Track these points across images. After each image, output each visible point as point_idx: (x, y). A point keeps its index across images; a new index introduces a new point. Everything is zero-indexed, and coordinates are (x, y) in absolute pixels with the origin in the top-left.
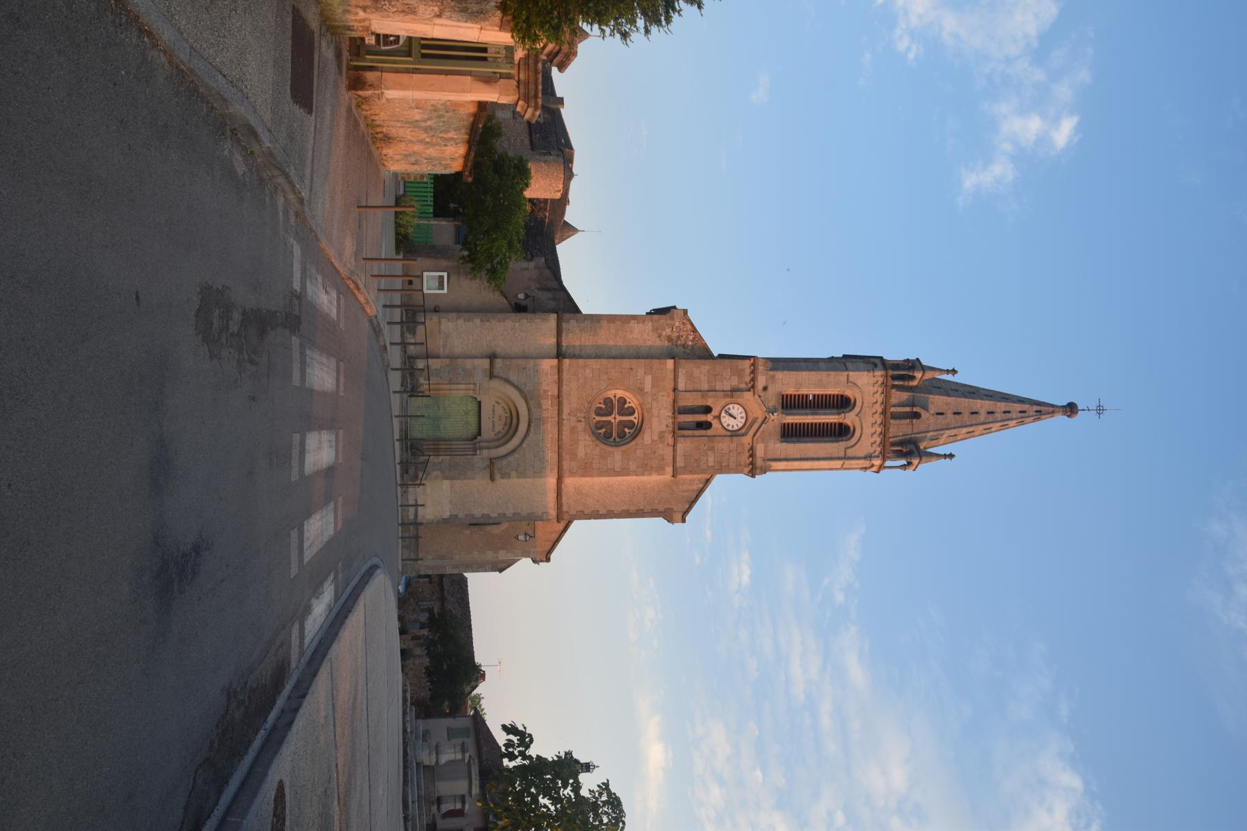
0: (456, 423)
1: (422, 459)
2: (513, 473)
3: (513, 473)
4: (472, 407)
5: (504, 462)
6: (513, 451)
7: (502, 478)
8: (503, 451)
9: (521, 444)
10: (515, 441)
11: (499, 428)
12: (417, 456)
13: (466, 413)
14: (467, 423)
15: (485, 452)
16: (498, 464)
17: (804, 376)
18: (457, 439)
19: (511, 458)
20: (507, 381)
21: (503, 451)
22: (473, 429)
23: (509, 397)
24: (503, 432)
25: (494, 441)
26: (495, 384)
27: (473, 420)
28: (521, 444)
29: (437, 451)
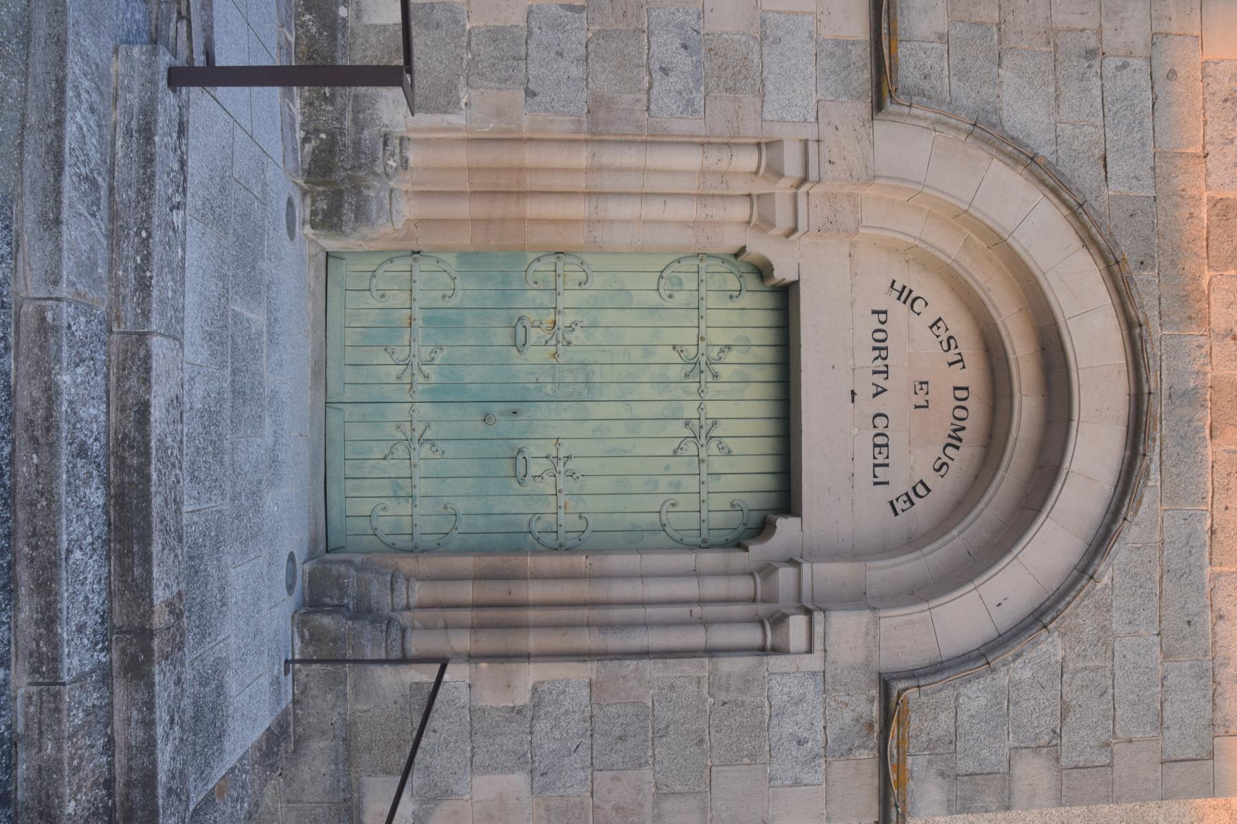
0: (642, 430)
1: (395, 683)
2: (1033, 773)
3: (1033, 773)
4: (741, 324)
5: (975, 696)
6: (1037, 619)
7: (959, 805)
8: (964, 617)
9: (1084, 570)
10: (1051, 545)
11: (914, 460)
12: (408, 580)
13: (699, 367)
14: (702, 432)
15: (846, 632)
16: (927, 713)
17: (185, 35)
18: (634, 541)
19: (1021, 669)
20: (988, 131)
21: (964, 617)
22: (743, 471)
23: (963, 219)
24: (944, 488)
25: (886, 550)
26: (905, 144)
27: (743, 413)
28: (1084, 570)
29: (502, 627)
